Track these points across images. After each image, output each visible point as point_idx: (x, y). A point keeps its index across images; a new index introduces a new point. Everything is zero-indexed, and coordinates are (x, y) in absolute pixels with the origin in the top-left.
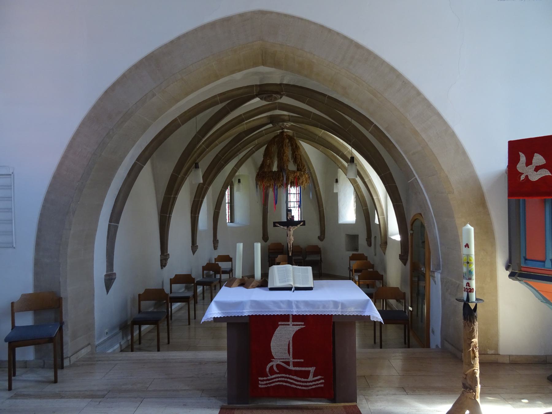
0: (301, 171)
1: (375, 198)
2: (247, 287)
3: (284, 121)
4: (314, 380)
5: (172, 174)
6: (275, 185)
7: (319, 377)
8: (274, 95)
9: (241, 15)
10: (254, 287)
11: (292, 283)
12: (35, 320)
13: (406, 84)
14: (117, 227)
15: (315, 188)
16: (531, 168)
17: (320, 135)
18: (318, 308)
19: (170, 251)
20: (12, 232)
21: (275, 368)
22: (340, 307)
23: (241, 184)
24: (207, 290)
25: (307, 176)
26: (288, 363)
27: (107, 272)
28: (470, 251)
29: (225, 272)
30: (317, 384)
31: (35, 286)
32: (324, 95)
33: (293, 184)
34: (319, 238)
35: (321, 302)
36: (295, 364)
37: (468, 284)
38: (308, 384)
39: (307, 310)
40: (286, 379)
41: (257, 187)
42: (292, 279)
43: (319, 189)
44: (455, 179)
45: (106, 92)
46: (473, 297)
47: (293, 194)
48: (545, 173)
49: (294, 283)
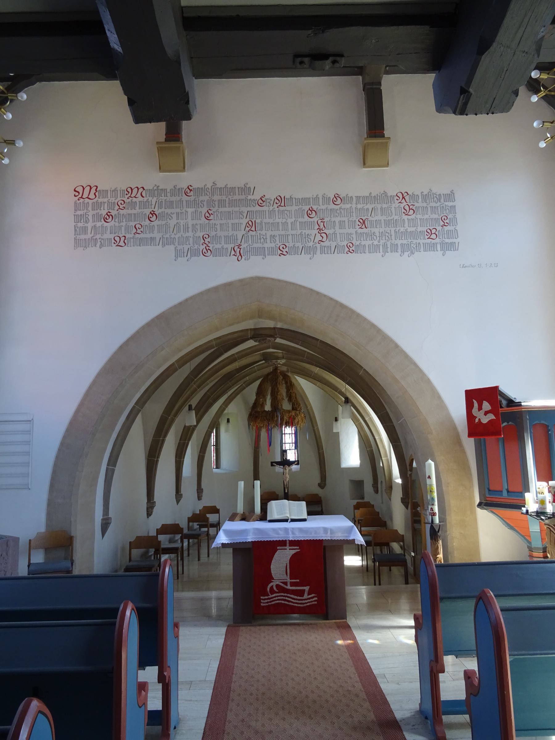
0: (296, 410)
1: (377, 437)
2: (248, 521)
3: (277, 358)
4: (308, 599)
5: (162, 416)
6: (268, 426)
7: (313, 595)
8: (268, 338)
9: (241, 281)
10: (254, 521)
11: (288, 516)
12: (46, 559)
13: (386, 338)
14: (113, 471)
15: (313, 427)
16: (482, 412)
17: (316, 372)
18: (311, 534)
19: (156, 498)
20: (28, 474)
21: (275, 588)
22: (329, 533)
23: (230, 425)
24: (194, 544)
25: (302, 415)
26: (286, 583)
27: (103, 516)
28: (431, 482)
29: (213, 526)
30: (312, 602)
31: (48, 526)
32: (317, 340)
33: (287, 424)
34: (319, 485)
35: (312, 528)
36: (292, 584)
37: (432, 509)
38: (303, 602)
39: (301, 536)
40: (284, 598)
41: (249, 428)
42: (288, 512)
43: (318, 428)
44: (432, 420)
45: (121, 347)
46: (437, 520)
47: (288, 435)
48: (491, 417)
49: (290, 515)
